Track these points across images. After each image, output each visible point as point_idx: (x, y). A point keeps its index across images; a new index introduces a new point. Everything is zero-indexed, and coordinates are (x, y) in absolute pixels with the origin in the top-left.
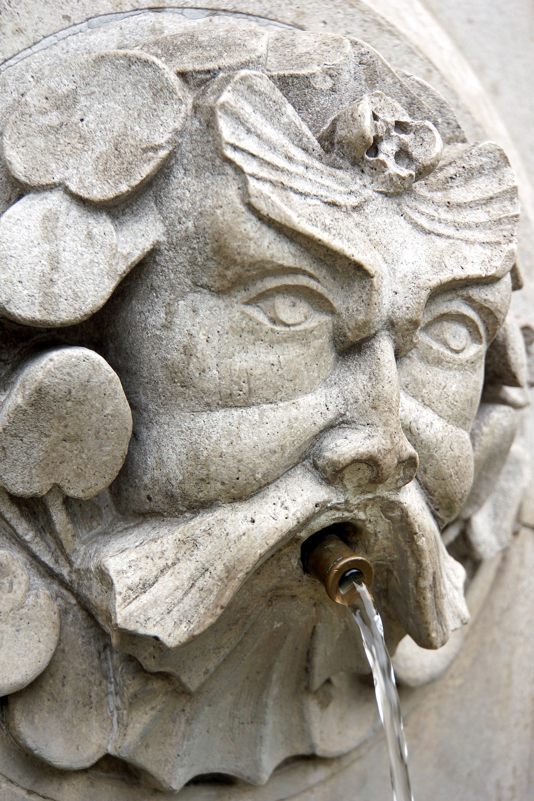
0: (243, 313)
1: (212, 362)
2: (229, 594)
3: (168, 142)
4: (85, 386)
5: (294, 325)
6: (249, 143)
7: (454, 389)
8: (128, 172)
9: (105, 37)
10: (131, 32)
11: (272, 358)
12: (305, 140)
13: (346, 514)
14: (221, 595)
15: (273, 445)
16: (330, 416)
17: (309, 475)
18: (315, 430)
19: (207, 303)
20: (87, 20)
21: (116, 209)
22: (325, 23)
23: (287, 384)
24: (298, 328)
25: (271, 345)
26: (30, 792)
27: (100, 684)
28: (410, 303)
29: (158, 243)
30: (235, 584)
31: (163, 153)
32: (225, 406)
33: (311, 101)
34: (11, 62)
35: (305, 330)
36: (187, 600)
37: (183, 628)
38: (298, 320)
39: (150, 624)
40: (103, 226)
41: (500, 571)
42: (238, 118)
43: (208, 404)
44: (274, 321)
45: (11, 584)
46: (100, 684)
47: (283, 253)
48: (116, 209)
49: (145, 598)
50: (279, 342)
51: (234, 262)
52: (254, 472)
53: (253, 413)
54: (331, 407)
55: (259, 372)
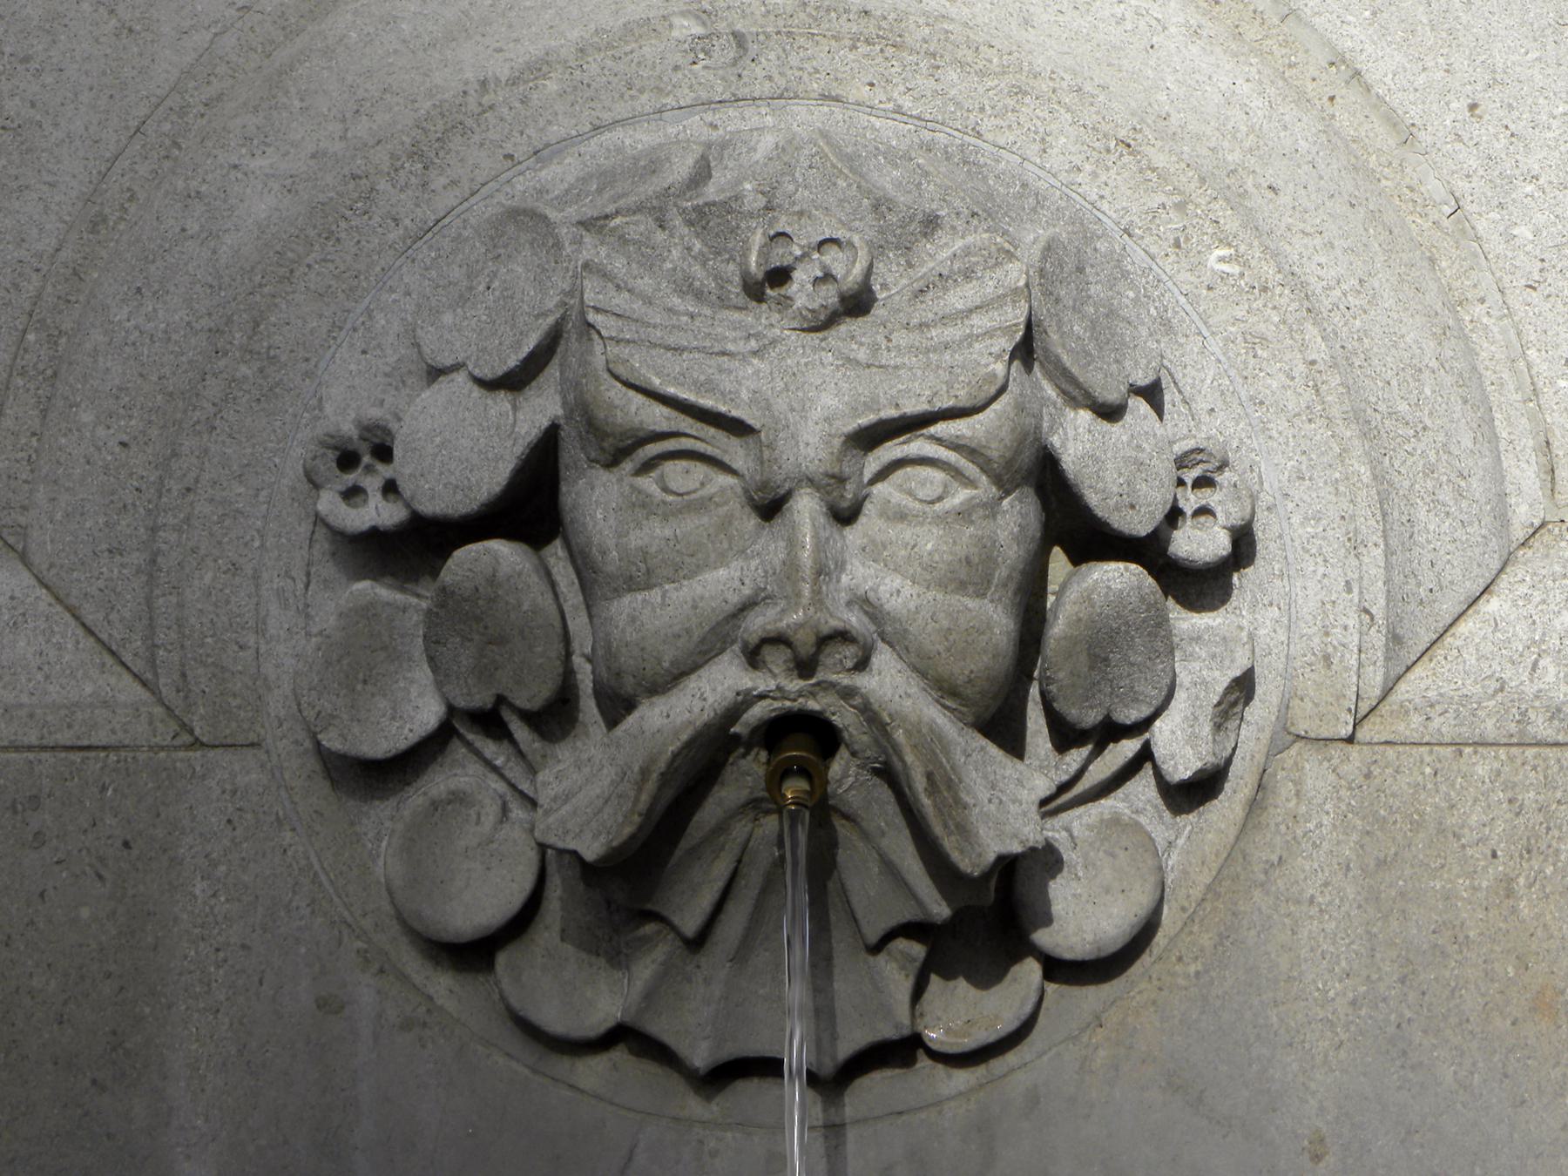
0: (632, 486)
1: (611, 543)
2: (645, 798)
3: (556, 306)
4: (492, 580)
5: (688, 493)
6: (620, 301)
7: (929, 546)
8: (518, 345)
9: (559, 169)
10: (593, 157)
11: (668, 532)
12: (697, 284)
13: (788, 704)
14: (637, 800)
15: (676, 629)
16: (747, 591)
17: (736, 661)
18: (729, 608)
19: (603, 477)
20: (535, 153)
21: (515, 381)
22: (872, 85)
23: (687, 560)
24: (693, 496)
25: (665, 518)
26: (535, 1071)
27: (611, 939)
28: (823, 455)
29: (557, 417)
30: (651, 785)
31: (551, 320)
32: (630, 590)
33: (738, 227)
34: (446, 221)
35: (702, 498)
36: (608, 810)
37: (603, 839)
38: (692, 487)
39: (568, 839)
40: (501, 402)
41: (1255, 805)
42: (605, 275)
43: (616, 590)
44: (666, 490)
45: (479, 815)
46: (611, 939)
47: (658, 417)
48: (515, 381)
49: (567, 808)
50: (673, 514)
51: (608, 435)
52: (659, 661)
53: (655, 595)
54: (747, 581)
55: (653, 550)
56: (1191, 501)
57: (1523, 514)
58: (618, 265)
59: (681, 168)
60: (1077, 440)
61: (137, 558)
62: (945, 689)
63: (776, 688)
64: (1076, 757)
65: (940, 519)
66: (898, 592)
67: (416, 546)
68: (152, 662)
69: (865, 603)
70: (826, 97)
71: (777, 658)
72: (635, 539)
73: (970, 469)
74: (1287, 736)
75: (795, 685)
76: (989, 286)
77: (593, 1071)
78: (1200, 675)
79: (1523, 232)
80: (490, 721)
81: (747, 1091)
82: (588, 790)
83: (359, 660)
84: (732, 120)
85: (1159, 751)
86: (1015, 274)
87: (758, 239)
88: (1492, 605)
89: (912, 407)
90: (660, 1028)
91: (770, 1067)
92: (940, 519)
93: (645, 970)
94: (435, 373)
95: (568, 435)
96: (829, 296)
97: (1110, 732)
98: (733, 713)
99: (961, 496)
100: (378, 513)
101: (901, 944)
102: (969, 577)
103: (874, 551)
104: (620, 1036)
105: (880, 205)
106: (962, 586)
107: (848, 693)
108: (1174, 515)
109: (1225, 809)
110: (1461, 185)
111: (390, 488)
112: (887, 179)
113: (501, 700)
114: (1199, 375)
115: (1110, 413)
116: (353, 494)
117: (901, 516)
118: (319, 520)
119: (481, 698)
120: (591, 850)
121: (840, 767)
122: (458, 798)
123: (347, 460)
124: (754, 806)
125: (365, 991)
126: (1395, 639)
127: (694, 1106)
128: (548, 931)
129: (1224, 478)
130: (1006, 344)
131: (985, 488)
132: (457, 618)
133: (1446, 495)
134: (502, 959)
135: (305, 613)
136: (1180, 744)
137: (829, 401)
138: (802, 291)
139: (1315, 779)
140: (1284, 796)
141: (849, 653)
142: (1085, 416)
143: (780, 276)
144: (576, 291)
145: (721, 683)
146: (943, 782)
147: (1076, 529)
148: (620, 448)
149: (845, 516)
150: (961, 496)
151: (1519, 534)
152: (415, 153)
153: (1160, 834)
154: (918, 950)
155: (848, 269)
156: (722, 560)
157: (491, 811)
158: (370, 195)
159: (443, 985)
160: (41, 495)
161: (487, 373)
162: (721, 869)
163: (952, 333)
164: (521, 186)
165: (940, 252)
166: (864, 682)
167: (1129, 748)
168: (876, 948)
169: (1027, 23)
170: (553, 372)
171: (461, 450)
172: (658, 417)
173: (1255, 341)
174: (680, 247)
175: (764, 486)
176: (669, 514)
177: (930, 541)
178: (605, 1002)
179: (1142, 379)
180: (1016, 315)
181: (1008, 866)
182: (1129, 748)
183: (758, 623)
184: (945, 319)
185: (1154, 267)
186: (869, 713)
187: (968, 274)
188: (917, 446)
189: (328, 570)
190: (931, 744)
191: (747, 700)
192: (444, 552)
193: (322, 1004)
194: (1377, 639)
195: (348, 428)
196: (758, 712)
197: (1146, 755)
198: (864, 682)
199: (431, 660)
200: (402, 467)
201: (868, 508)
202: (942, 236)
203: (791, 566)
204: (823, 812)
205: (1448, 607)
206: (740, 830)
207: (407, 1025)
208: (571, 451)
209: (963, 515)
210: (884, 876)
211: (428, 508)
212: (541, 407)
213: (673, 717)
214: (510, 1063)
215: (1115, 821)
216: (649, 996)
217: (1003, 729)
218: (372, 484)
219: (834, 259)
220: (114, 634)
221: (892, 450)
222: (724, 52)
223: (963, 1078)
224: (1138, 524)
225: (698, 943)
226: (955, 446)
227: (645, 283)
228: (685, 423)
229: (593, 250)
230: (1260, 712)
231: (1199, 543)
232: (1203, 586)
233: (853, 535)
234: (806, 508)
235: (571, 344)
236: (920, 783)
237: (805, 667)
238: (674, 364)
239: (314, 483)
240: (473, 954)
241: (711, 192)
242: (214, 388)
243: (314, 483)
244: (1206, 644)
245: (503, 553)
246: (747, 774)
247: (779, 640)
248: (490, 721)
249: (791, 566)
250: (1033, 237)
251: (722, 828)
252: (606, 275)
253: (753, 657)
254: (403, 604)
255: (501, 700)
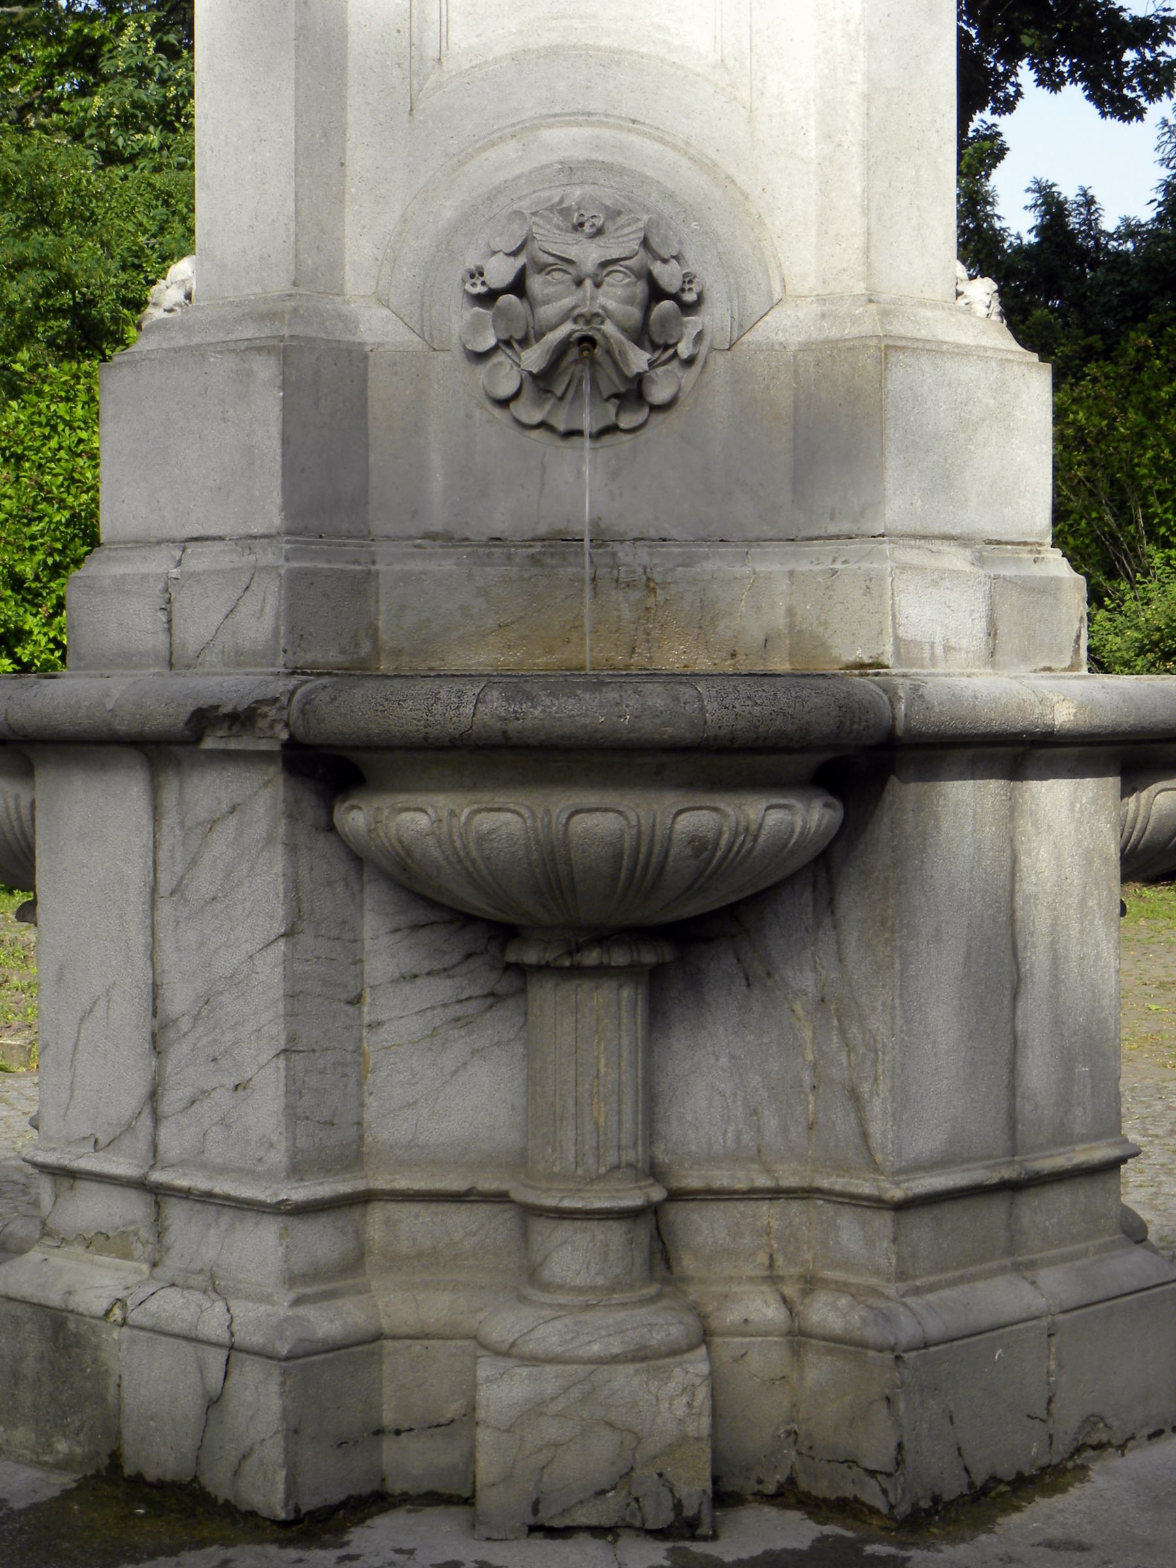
6: (542, 231)
21: (515, 254)
40: (511, 259)
41: (704, 367)
47: (551, 260)
48: (515, 254)
56: (687, 286)
57: (777, 296)
58: (541, 222)
59: (556, 199)
60: (657, 268)
61: (418, 304)
62: (623, 330)
63: (580, 329)
64: (657, 354)
65: (622, 286)
66: (611, 305)
67: (488, 298)
68: (422, 331)
69: (603, 307)
70: (594, 183)
71: (581, 321)
72: (545, 292)
73: (629, 273)
74: (712, 349)
75: (585, 328)
76: (634, 228)
77: (535, 434)
78: (691, 332)
79: (777, 222)
80: (508, 343)
81: (575, 440)
82: (534, 358)
83: (476, 327)
84: (568, 189)
85: (679, 352)
86: (641, 225)
87: (576, 215)
88: (766, 318)
89: (614, 257)
90: (552, 421)
91: (579, 433)
92: (622, 286)
93: (548, 407)
94: (495, 253)
95: (528, 266)
96: (593, 230)
97: (667, 347)
98: (570, 335)
99: (627, 280)
100: (480, 289)
101: (613, 400)
102: (630, 301)
103: (605, 295)
104: (543, 425)
105: (607, 208)
106: (628, 304)
107: (599, 330)
108: (683, 290)
109: (697, 368)
110: (761, 211)
111: (483, 283)
112: (608, 203)
113: (511, 337)
114: (690, 255)
115: (665, 261)
116: (474, 285)
117: (612, 285)
118: (465, 291)
119: (505, 336)
120: (535, 370)
121: (598, 351)
122: (500, 364)
123: (472, 276)
124: (576, 362)
125: (477, 413)
126: (741, 326)
127: (560, 443)
128: (523, 398)
129: (696, 280)
130: (638, 242)
131: (633, 279)
132: (503, 315)
133: (755, 289)
134: (512, 405)
135: (461, 316)
136: (684, 349)
137: (594, 255)
138: (587, 229)
139: (719, 362)
140: (711, 362)
141: (599, 320)
142: (659, 262)
143: (581, 225)
144: (530, 230)
145: (567, 328)
146: (623, 353)
147: (656, 293)
148: (542, 268)
149: (598, 285)
150: (627, 280)
151: (775, 301)
152: (488, 199)
153: (680, 374)
154: (616, 401)
155: (599, 222)
156: (567, 296)
157: (508, 368)
158: (477, 210)
159: (497, 412)
160: (392, 290)
161: (508, 251)
162: (567, 379)
163: (625, 239)
164: (515, 207)
165: (622, 220)
166: (603, 327)
167: (671, 351)
168: (608, 399)
169: (645, 165)
170: (524, 252)
171: (500, 272)
172: (551, 260)
173: (703, 246)
174: (556, 219)
175: (578, 277)
176: (554, 285)
177: (619, 292)
178: (537, 417)
179: (674, 254)
180: (642, 235)
181: (639, 374)
182: (671, 351)
183: (576, 312)
184: (623, 236)
185: (1007, 1262)
186: (605, 336)
187: (629, 225)
188: (616, 268)
189: (466, 305)
190: (620, 343)
191: (574, 331)
192: (496, 299)
193: (467, 416)
194: (736, 325)
195: (473, 267)
196: (576, 335)
197: (675, 355)
198: (603, 327)
199: (494, 327)
200: (487, 277)
201: (605, 284)
202: (623, 216)
203: (584, 298)
204: (594, 363)
205: (755, 318)
206: (572, 368)
207: (488, 422)
208: (529, 271)
209: (628, 285)
210: (610, 383)
211: (493, 286)
212: (521, 260)
213: (554, 337)
214: (514, 432)
215: (668, 371)
216: (550, 413)
217: (639, 343)
218: (478, 282)
219: (595, 221)
220: (412, 324)
221: (610, 268)
222: (567, 172)
223: (628, 437)
224: (673, 289)
225: (561, 398)
226: (626, 267)
227: (548, 227)
228: (558, 261)
229: (534, 219)
230: (706, 343)
231: (689, 297)
232: (689, 308)
233: (600, 291)
234: (588, 283)
235: (530, 244)
236: (617, 353)
237: (588, 322)
238: (555, 246)
239: (464, 282)
240: (504, 403)
241: (564, 205)
242: (438, 260)
243: (464, 282)
244: (693, 324)
245: (511, 298)
246: (574, 353)
247: (581, 315)
248: (508, 343)
249: (584, 298)
250: (645, 217)
251: (567, 368)
252: (538, 225)
253: (575, 321)
254: (486, 313)
255: (511, 337)
